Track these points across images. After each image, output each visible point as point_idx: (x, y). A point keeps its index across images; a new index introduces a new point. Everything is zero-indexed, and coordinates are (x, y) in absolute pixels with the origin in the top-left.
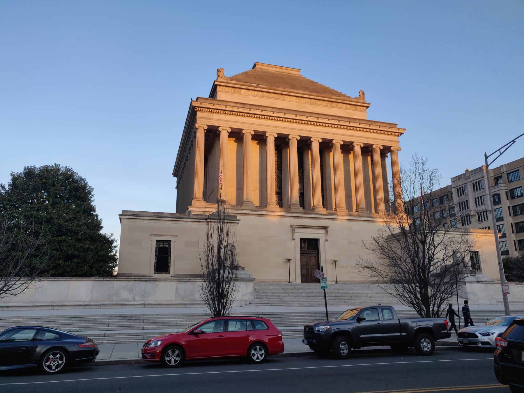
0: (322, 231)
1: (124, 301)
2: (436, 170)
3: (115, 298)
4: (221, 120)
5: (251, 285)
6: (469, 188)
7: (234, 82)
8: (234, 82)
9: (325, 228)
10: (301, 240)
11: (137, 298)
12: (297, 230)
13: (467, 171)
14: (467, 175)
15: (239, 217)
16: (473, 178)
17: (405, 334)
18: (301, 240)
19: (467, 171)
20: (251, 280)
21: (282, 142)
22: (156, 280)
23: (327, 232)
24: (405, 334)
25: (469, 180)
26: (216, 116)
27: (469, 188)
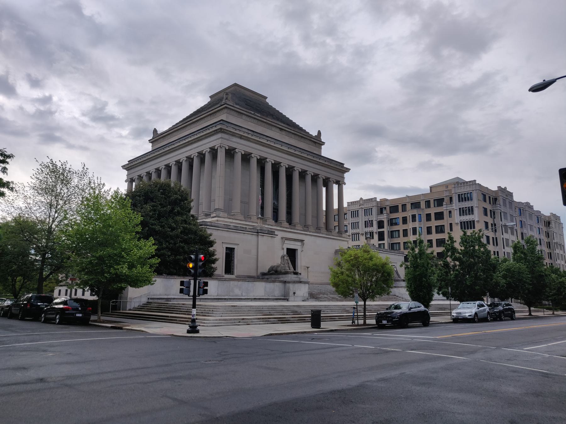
0: (299, 243)
1: (236, 296)
2: (124, 167)
3: (231, 294)
4: (238, 143)
5: (307, 285)
6: (361, 213)
7: (238, 107)
8: (238, 107)
9: (302, 241)
10: (287, 249)
11: (244, 294)
12: (286, 242)
13: (361, 199)
14: (361, 202)
15: (276, 233)
16: (366, 206)
17: (81, 315)
18: (287, 249)
19: (361, 199)
20: (307, 283)
21: (276, 167)
22: (225, 280)
23: (303, 244)
24: (81, 315)
25: (361, 207)
26: (235, 139)
27: (361, 213)
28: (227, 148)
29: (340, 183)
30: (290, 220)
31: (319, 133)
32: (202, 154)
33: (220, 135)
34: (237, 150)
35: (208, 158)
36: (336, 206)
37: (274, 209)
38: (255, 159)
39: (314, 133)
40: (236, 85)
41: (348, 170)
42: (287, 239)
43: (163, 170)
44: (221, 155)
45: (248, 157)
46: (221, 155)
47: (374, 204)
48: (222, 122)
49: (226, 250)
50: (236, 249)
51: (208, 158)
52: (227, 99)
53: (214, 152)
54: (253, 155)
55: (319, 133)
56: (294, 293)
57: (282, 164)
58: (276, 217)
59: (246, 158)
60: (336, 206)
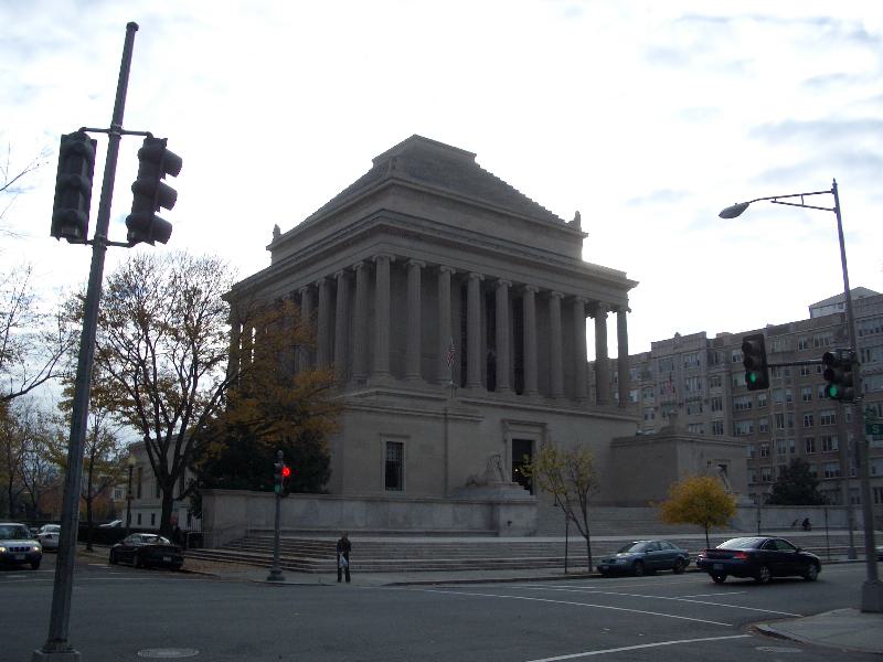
0: (538, 430)
9: (543, 426)
10: (515, 441)
18: (515, 441)
19: (677, 335)
28: (563, 296)
29: (622, 309)
30: (519, 388)
31: (578, 216)
32: (351, 271)
33: (381, 237)
34: (442, 269)
35: (361, 278)
36: (613, 353)
37: (488, 365)
38: (582, 304)
39: (568, 218)
40: (415, 137)
41: (633, 284)
42: (512, 422)
43: (322, 288)
44: (383, 272)
45: (404, 265)
46: (383, 272)
47: (703, 344)
48: (382, 213)
49: (388, 448)
50: (405, 447)
51: (361, 278)
52: (394, 168)
53: (370, 266)
54: (472, 275)
55: (578, 216)
56: (509, 522)
57: (500, 281)
58: (491, 384)
59: (431, 274)
60: (613, 353)
